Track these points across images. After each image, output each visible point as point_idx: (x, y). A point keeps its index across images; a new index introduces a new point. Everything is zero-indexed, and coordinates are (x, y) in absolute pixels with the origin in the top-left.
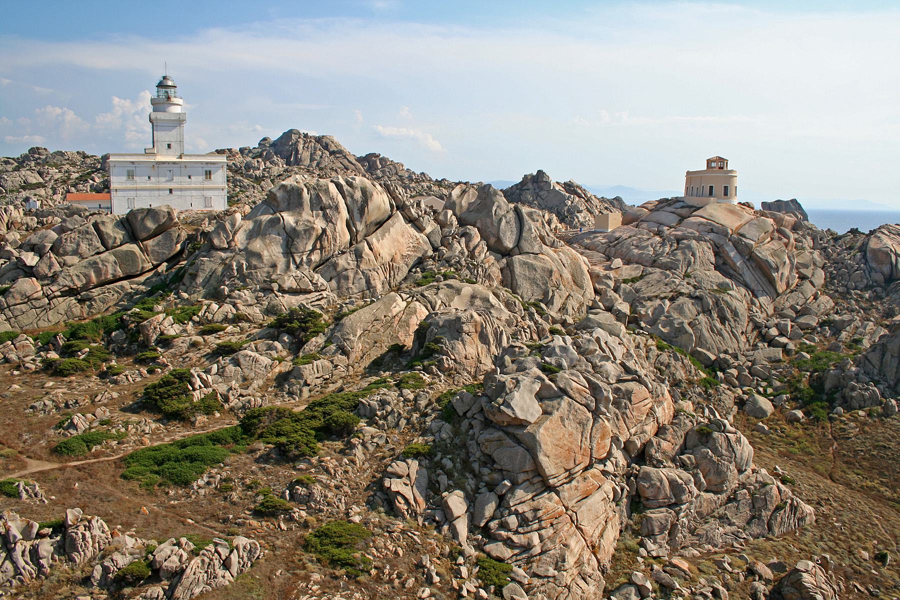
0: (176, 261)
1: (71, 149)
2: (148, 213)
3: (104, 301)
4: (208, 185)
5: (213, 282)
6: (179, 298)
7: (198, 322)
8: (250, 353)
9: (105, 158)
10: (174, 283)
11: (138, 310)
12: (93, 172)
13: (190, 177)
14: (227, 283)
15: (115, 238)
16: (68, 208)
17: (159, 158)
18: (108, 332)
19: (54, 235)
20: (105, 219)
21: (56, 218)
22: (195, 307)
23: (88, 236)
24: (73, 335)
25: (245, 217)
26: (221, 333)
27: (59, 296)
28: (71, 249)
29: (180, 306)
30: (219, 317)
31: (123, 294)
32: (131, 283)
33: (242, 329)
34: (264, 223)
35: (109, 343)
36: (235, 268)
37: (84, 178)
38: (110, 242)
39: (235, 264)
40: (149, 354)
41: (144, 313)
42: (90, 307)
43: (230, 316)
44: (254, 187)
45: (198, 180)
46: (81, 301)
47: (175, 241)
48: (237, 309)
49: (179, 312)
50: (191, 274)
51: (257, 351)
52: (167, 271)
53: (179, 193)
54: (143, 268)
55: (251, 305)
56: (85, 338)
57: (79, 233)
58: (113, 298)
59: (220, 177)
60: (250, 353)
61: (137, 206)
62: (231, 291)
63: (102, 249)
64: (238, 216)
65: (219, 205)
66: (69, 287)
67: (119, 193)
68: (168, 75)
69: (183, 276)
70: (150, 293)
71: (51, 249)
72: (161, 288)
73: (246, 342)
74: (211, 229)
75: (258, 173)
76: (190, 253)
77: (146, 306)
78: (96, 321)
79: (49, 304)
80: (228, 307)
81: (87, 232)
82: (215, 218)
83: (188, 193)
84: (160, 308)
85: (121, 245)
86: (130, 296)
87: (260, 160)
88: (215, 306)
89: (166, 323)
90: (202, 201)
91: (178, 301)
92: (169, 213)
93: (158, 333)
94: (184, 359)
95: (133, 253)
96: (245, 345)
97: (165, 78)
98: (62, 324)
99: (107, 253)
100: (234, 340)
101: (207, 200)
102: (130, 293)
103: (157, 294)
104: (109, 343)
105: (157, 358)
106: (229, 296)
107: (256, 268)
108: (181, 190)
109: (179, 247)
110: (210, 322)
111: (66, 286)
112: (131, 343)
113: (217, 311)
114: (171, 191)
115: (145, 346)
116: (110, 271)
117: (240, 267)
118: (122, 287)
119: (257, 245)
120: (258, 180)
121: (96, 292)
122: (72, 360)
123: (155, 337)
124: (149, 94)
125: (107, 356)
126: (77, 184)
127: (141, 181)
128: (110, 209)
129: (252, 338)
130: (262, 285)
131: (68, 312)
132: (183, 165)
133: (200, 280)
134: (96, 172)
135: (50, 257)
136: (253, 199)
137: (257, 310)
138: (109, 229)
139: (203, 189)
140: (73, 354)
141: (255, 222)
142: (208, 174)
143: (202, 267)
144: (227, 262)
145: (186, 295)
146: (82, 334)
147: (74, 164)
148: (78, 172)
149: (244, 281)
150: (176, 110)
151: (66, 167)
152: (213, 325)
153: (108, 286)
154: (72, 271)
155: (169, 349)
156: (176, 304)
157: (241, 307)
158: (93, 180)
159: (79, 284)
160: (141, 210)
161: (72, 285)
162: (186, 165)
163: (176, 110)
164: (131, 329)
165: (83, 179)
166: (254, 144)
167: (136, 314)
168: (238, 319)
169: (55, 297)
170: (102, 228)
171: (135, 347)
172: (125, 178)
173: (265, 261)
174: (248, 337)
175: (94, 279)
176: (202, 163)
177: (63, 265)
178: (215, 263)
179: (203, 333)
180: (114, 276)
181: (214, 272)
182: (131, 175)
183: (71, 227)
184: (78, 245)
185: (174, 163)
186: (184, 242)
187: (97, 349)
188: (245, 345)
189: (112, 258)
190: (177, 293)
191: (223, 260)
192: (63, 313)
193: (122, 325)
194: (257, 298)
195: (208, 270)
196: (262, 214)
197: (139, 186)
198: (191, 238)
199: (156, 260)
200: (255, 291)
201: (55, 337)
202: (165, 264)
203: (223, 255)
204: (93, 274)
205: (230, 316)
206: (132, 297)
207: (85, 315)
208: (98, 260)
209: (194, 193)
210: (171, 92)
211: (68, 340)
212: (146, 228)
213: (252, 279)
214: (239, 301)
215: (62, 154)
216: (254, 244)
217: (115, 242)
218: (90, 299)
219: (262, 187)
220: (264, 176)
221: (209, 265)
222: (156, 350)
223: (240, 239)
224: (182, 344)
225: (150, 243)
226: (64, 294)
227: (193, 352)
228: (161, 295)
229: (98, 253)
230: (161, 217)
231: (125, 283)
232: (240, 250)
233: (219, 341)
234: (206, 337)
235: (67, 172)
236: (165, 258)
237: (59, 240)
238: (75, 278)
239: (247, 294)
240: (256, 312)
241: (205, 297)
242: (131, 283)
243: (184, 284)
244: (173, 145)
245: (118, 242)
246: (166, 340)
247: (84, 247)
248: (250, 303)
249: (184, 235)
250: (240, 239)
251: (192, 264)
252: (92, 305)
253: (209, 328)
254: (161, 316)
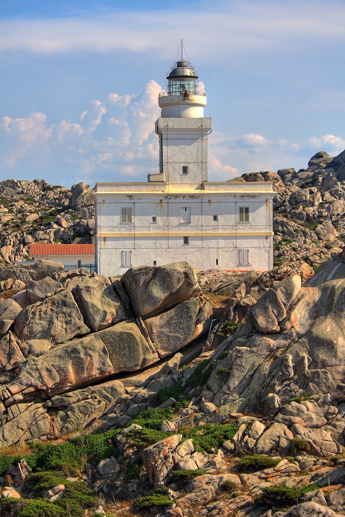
0: (196, 350)
1: (25, 177)
2: (154, 275)
3: (85, 412)
4: (243, 230)
5: (255, 385)
6: (201, 410)
7: (232, 452)
8: (318, 506)
9: (77, 190)
10: (194, 386)
11: (139, 427)
12: (59, 212)
13: (215, 218)
14: (278, 388)
15: (105, 313)
16: (35, 267)
17: (171, 189)
18: (94, 461)
19: (16, 307)
20: (91, 283)
21: (18, 281)
22: (226, 427)
23: (65, 309)
24: (42, 462)
25: (307, 283)
26: (270, 470)
27: (21, 402)
28: (39, 328)
29: (201, 423)
30: (265, 444)
31: (114, 401)
32: (126, 384)
33: (303, 466)
34: (338, 293)
35: (94, 479)
36: (291, 364)
37: (45, 221)
38: (98, 319)
39: (290, 358)
40: (156, 499)
41: (150, 433)
42: (65, 419)
43: (284, 443)
44: (305, 234)
45: (228, 220)
46: (52, 410)
47: (194, 318)
48: (296, 432)
49: (201, 432)
50: (220, 373)
51: (329, 503)
52: (181, 366)
53: (199, 243)
54: (145, 360)
55: (317, 427)
56: (58, 468)
57: (53, 303)
58: (99, 407)
59: (262, 217)
60: (318, 506)
61: (137, 263)
62: (283, 402)
63: (85, 329)
64: (297, 280)
65: (261, 263)
66: (35, 387)
67: (110, 244)
68: (185, 58)
69: (207, 376)
70: (155, 401)
71: (12, 328)
72: (171, 394)
73: (310, 488)
74: (251, 300)
75: (311, 210)
76: (220, 339)
77: (150, 421)
78: (75, 442)
79: (6, 412)
80: (279, 429)
81: (64, 303)
82: (256, 283)
83: (213, 243)
84: (172, 426)
85: (113, 324)
86: (124, 404)
87: (315, 189)
88: (259, 426)
89: (183, 450)
90: (234, 255)
91: (199, 415)
92: (187, 275)
93: (170, 465)
94: (210, 510)
95: (131, 336)
96: (309, 494)
97: (180, 64)
98: (23, 444)
99: (92, 336)
100: (291, 483)
101: (242, 255)
102: (125, 400)
103: (167, 403)
104: (94, 479)
105: (168, 506)
106: (281, 410)
107: (324, 365)
108: (202, 238)
109: (200, 328)
110: (251, 451)
111: (31, 385)
112: (127, 481)
113: (266, 435)
114: (186, 240)
115: (149, 484)
116: (97, 365)
117: (299, 362)
118: (113, 390)
119: (327, 328)
120: (312, 221)
121: (74, 396)
122: (40, 502)
123: (165, 472)
124: (157, 90)
125: (92, 499)
126: (35, 230)
127: (141, 223)
128: (95, 267)
129: (319, 481)
130: (334, 394)
131: (33, 426)
132: (206, 199)
133: (234, 383)
134: (69, 213)
135: (10, 341)
136: (304, 253)
137: (328, 435)
138: (96, 299)
139: (236, 237)
140: (40, 493)
141: (324, 290)
142: (245, 212)
143: (238, 361)
144: (278, 354)
145: (211, 406)
146: (54, 461)
147: (30, 200)
148: (36, 212)
149: (305, 386)
150: (196, 113)
151: (19, 205)
152: (258, 457)
153: (92, 388)
154: (41, 363)
155: (186, 492)
156: (196, 420)
157: (302, 430)
158: (59, 223)
159: (50, 384)
160: (145, 270)
161: (39, 384)
162: (210, 199)
163: (196, 113)
164: (128, 456)
165: (43, 223)
166: (300, 163)
167: (137, 434)
168: (295, 449)
169: (15, 402)
170: (87, 297)
171: (133, 486)
172: (117, 219)
173: (340, 354)
174: (313, 479)
175: (72, 377)
176: (234, 195)
177: (29, 352)
178: (259, 356)
179: (239, 469)
180: (102, 372)
181: (256, 370)
182: (127, 215)
183: (41, 295)
184: (51, 322)
185: (192, 196)
186: (208, 321)
187: (78, 487)
188: (309, 494)
189: (99, 345)
190: (198, 402)
191: (272, 351)
192: (25, 427)
193: (114, 449)
194: (327, 415)
195: (248, 367)
196: (334, 277)
197: (138, 232)
198: (218, 316)
199: (166, 349)
200: (324, 403)
201: (15, 463)
202: (179, 356)
203: (272, 342)
204: (70, 369)
205: (284, 443)
206: (128, 406)
207: (57, 432)
208: (79, 347)
209: (222, 243)
210: (189, 85)
211: (34, 470)
212: (151, 298)
213: (318, 384)
214: (297, 419)
215: (13, 184)
216: (323, 326)
217: (104, 319)
218: (65, 407)
219: (318, 234)
220: (320, 216)
221: (251, 359)
222: (166, 493)
223: (299, 317)
224: (206, 485)
225: (156, 321)
226: (29, 398)
227: (223, 499)
228: (174, 405)
229: (79, 336)
230: (175, 281)
231: (117, 383)
232: (300, 336)
233: (265, 485)
234: (245, 476)
235: (20, 211)
236: (179, 346)
237: (24, 315)
238: (44, 373)
239: (310, 408)
240: (325, 438)
241: (242, 411)
242: (126, 384)
243: (209, 389)
244: (191, 167)
245: (109, 319)
246: (183, 477)
247: (59, 326)
248: (315, 422)
249: (208, 310)
250: (299, 317)
251: (223, 356)
252: (67, 416)
253: (249, 463)
254: (176, 438)
